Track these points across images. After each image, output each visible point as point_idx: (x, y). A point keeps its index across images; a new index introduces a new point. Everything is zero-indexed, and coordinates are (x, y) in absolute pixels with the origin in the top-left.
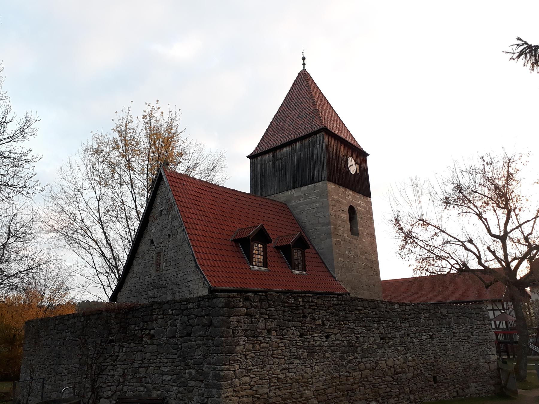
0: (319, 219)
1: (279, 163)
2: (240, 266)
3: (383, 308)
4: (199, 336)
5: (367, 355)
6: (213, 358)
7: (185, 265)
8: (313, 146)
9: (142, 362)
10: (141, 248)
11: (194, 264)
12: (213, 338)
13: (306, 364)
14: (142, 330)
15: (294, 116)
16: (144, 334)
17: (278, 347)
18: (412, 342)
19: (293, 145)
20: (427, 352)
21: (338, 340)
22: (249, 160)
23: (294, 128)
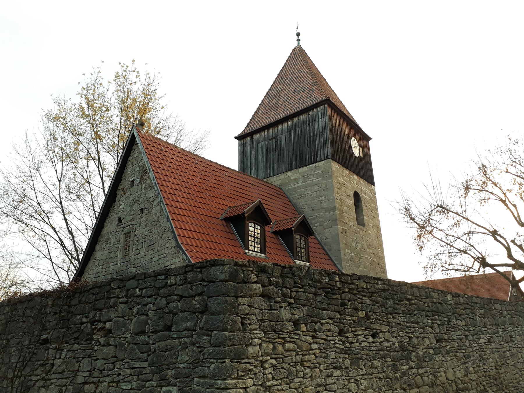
0: (321, 203)
2: (232, 249)
3: (435, 298)
4: (185, 330)
5: (424, 364)
6: (209, 367)
7: (162, 245)
8: (313, 121)
9: (90, 374)
10: (106, 229)
11: (173, 243)
12: (210, 333)
13: (348, 376)
14: (92, 322)
15: (289, 91)
16: (95, 328)
17: (310, 350)
18: (471, 347)
19: (290, 121)
20: (487, 360)
21: (388, 341)
22: (237, 141)
23: (290, 104)
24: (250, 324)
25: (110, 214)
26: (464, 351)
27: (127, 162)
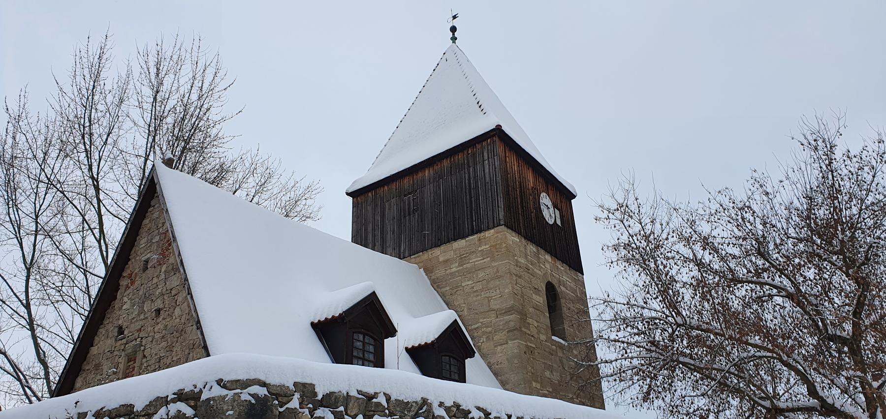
0: (489, 301)
1: (409, 202)
8: (475, 164)
22: (350, 200)
27: (140, 228)
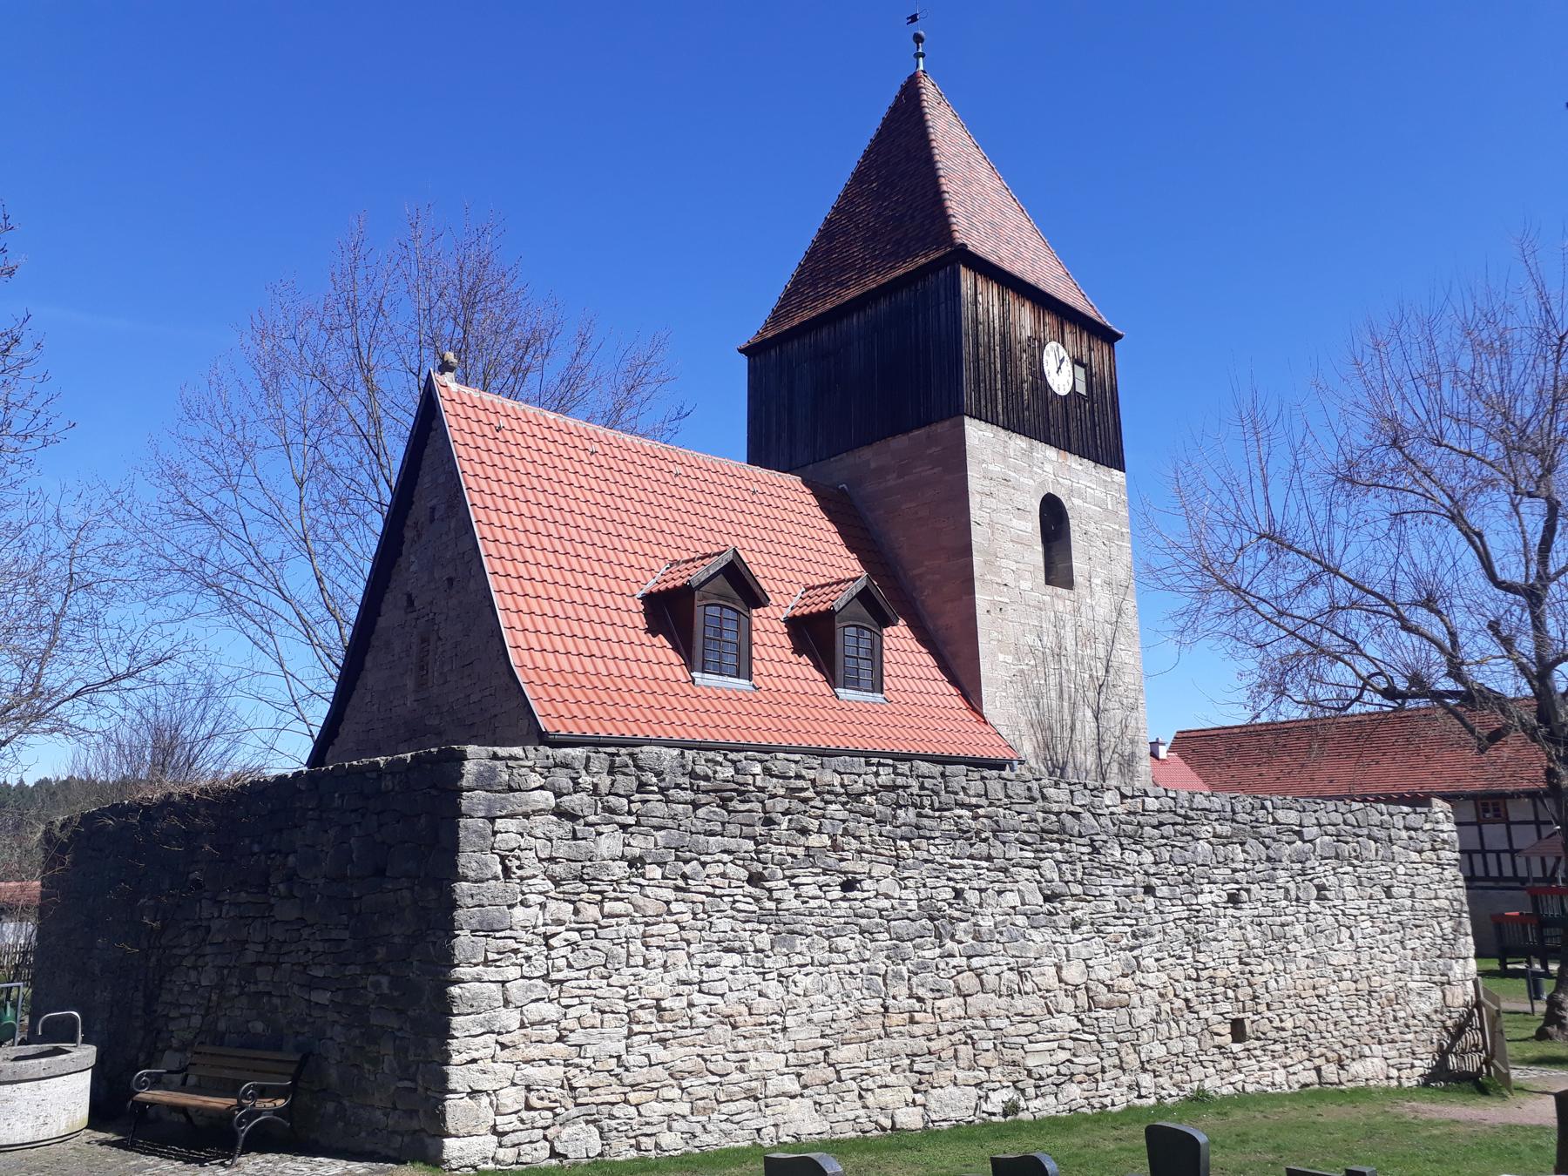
24: (518, 868)
25: (392, 585)
26: (1134, 922)
